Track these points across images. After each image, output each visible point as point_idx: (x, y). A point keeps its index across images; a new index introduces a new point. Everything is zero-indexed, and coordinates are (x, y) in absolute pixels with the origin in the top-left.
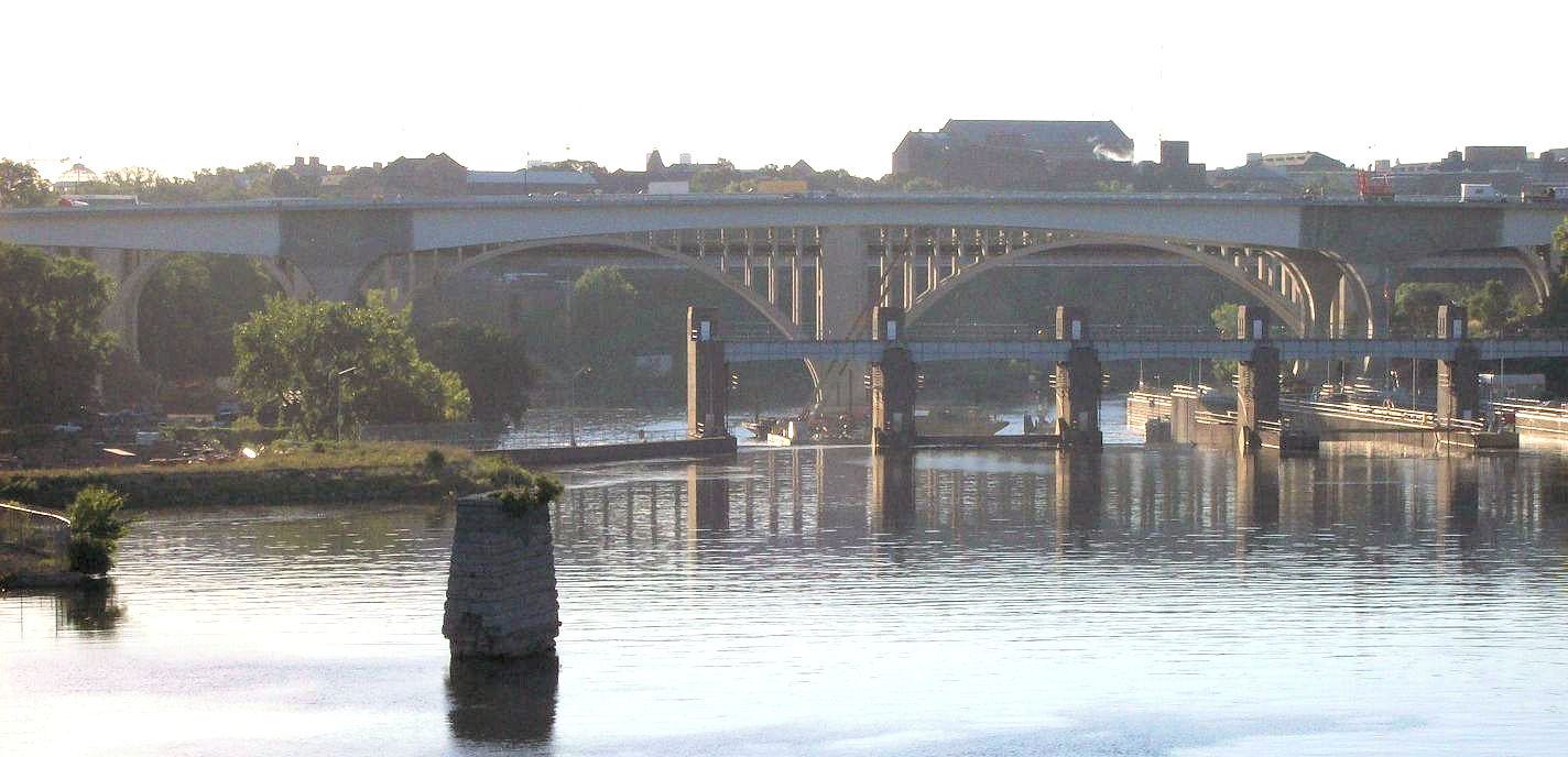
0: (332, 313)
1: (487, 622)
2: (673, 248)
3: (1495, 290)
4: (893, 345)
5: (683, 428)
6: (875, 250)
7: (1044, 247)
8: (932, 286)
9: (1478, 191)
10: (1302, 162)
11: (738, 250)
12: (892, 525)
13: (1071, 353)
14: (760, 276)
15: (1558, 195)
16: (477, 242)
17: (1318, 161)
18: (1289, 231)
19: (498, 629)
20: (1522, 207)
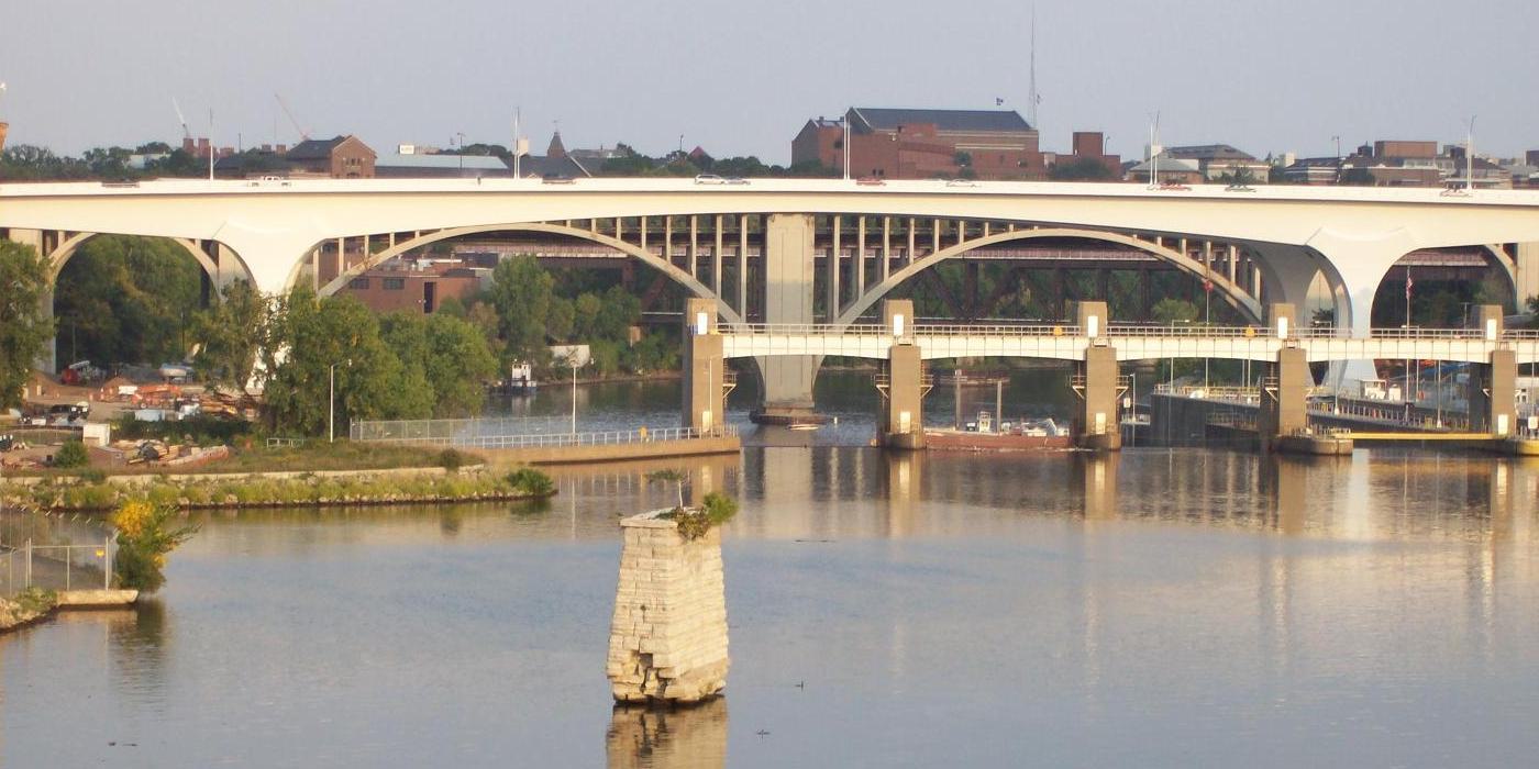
4: (901, 341)
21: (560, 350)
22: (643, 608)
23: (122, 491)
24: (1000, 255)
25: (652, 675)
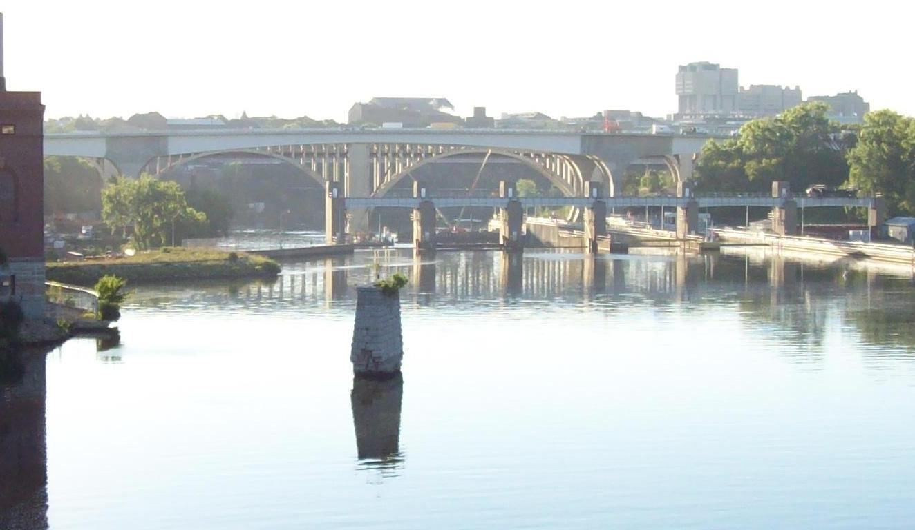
0: (150, 185)
1: (375, 354)
2: (279, 154)
3: (652, 174)
4: (424, 200)
5: (327, 238)
6: (373, 155)
7: (450, 154)
8: (399, 171)
9: (662, 129)
10: (533, 116)
11: (309, 155)
12: (802, 307)
13: (421, 204)
14: (319, 167)
15: (697, 131)
16: (178, 153)
17: (539, 116)
18: (575, 147)
19: (380, 357)
20: (682, 136)
21: (251, 205)
22: (367, 329)
23: (85, 273)
24: (450, 161)
25: (371, 361)
